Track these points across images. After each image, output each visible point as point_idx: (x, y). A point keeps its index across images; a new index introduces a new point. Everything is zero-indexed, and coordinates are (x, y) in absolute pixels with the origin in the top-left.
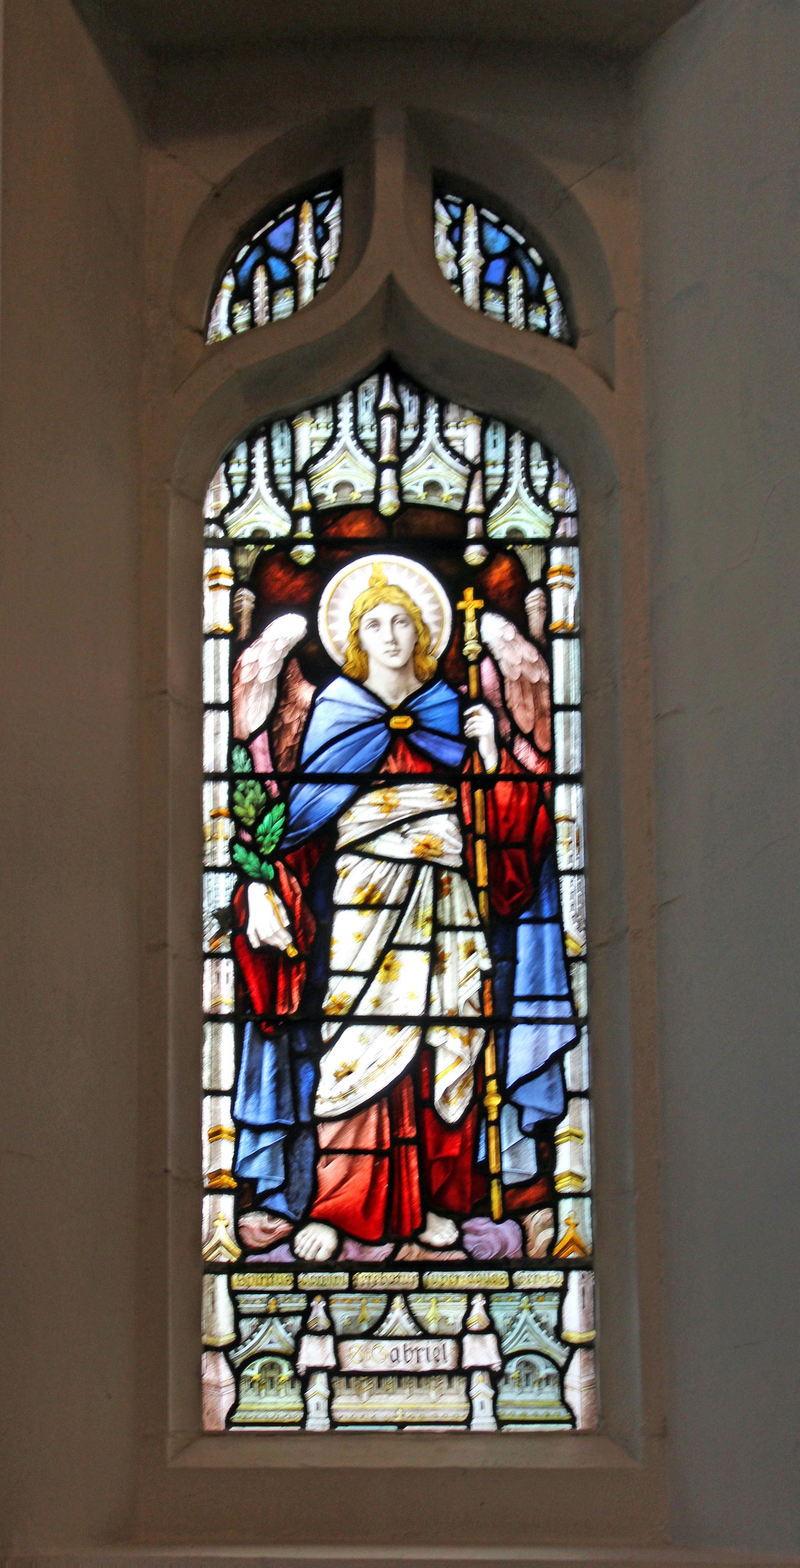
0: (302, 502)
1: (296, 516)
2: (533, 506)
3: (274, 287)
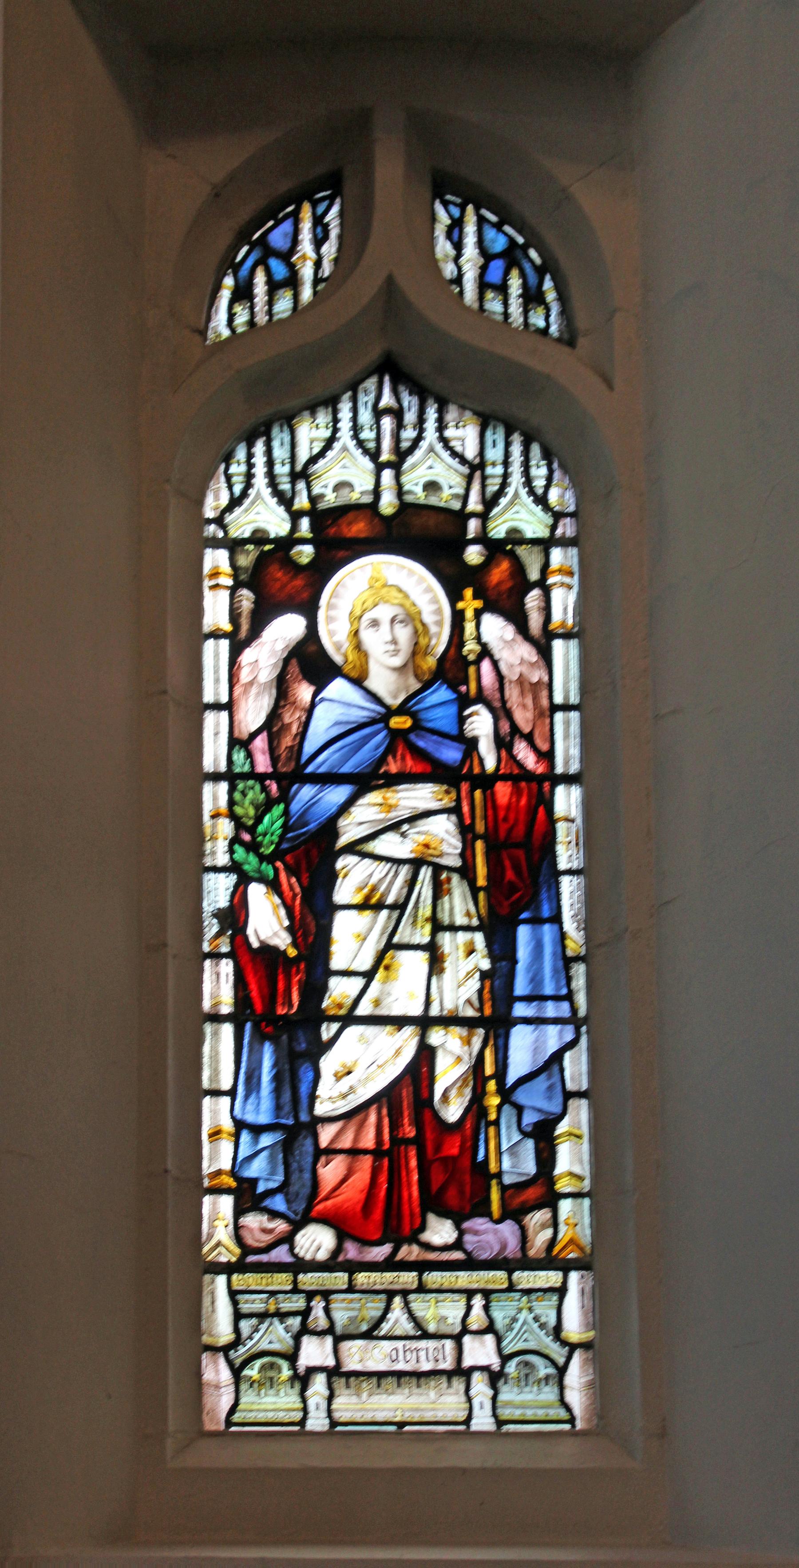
0: (302, 502)
1: (295, 516)
2: (533, 506)
3: (273, 287)
